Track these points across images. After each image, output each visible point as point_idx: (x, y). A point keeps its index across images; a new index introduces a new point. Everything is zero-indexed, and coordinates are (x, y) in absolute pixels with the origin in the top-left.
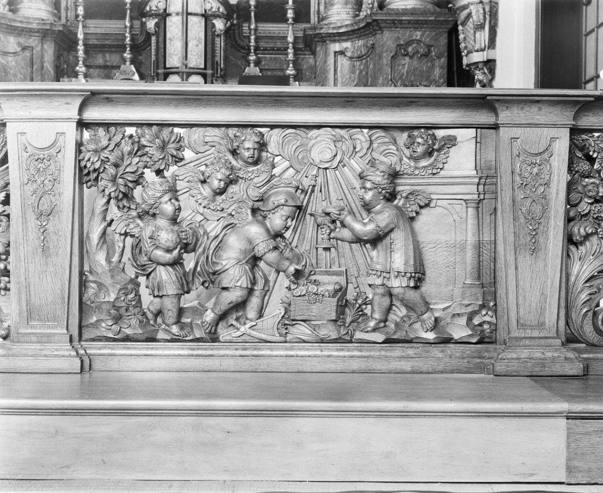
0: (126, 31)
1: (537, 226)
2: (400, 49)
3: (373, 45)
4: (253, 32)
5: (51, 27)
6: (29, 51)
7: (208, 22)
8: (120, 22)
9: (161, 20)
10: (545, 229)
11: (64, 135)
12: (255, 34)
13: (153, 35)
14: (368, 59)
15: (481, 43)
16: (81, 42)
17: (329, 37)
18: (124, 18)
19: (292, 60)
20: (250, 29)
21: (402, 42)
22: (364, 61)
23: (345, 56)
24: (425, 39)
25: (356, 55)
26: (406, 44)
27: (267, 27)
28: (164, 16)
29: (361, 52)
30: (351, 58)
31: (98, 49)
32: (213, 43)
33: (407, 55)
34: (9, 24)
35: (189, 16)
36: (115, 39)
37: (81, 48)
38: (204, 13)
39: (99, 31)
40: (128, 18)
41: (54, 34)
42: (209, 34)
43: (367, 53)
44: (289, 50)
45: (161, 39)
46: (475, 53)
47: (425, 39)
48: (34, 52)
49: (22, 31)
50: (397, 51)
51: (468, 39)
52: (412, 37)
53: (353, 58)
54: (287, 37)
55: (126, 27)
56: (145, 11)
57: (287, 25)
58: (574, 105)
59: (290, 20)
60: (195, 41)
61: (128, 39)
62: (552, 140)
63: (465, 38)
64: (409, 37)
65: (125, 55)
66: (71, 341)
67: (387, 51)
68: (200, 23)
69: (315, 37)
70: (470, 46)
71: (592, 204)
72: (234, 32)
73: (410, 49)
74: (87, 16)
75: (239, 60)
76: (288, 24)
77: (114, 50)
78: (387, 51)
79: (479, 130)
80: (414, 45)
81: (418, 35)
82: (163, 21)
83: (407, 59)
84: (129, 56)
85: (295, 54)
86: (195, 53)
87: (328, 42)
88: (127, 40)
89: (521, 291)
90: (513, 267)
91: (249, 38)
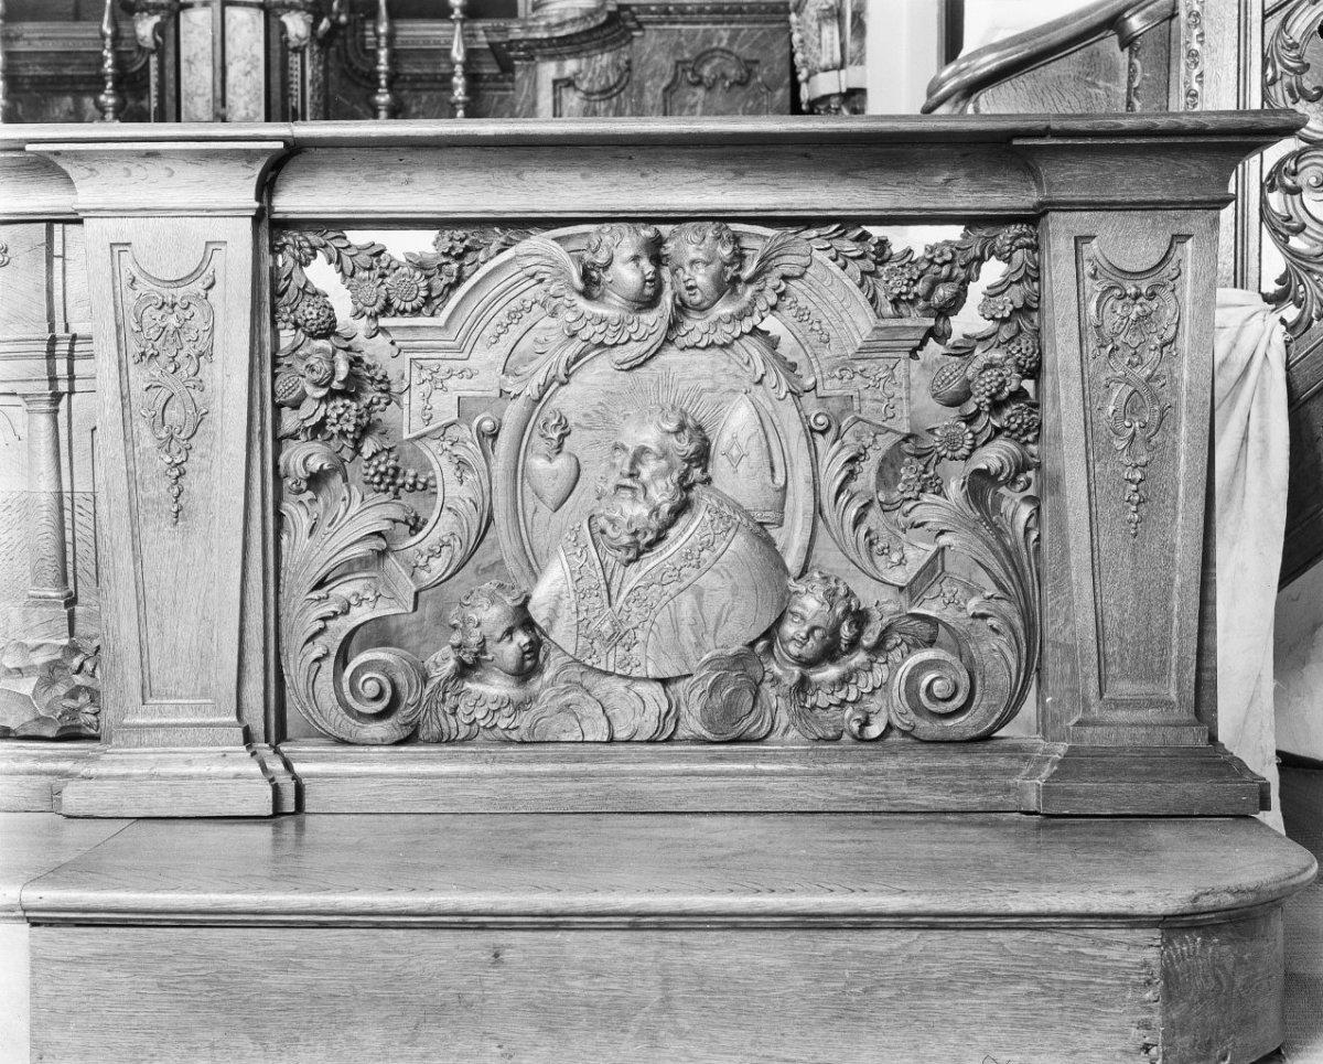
0: (104, 46)
1: (184, 453)
2: (684, 70)
3: (629, 62)
4: (383, 41)
7: (272, 20)
9: (169, 17)
10: (206, 463)
11: (223, 248)
12: (390, 44)
13: (153, 52)
14: (622, 94)
15: (832, 53)
17: (539, 47)
18: (101, 19)
19: (464, 102)
20: (377, 35)
21: (687, 56)
22: (614, 100)
23: (576, 89)
24: (740, 46)
25: (597, 87)
26: (698, 58)
27: (419, 29)
29: (608, 79)
30: (588, 93)
31: (50, 87)
32: (285, 67)
33: (699, 83)
36: (84, 64)
39: (50, 47)
40: (106, 17)
42: (276, 46)
43: (619, 81)
44: (455, 80)
45: (170, 60)
46: (821, 76)
47: (740, 46)
50: (676, 75)
51: (808, 42)
52: (711, 43)
53: (592, 94)
54: (449, 50)
55: (103, 36)
57: (451, 25)
58: (249, 162)
59: (457, 11)
60: (243, 63)
61: (110, 62)
62: (212, 247)
63: (802, 41)
64: (703, 45)
65: (102, 98)
66: (248, 738)
67: (653, 75)
68: (254, 23)
69: (510, 49)
70: (811, 60)
71: (322, 400)
72: (345, 44)
73: (706, 71)
74: (472, 12)
75: (358, 103)
76: (452, 21)
78: (653, 75)
79: (57, 228)
80: (716, 61)
81: (723, 33)
82: (173, 20)
83: (700, 92)
84: (111, 101)
85: (469, 90)
86: (242, 91)
87: (537, 59)
88: (106, 66)
89: (151, 612)
90: (128, 554)
91: (374, 55)
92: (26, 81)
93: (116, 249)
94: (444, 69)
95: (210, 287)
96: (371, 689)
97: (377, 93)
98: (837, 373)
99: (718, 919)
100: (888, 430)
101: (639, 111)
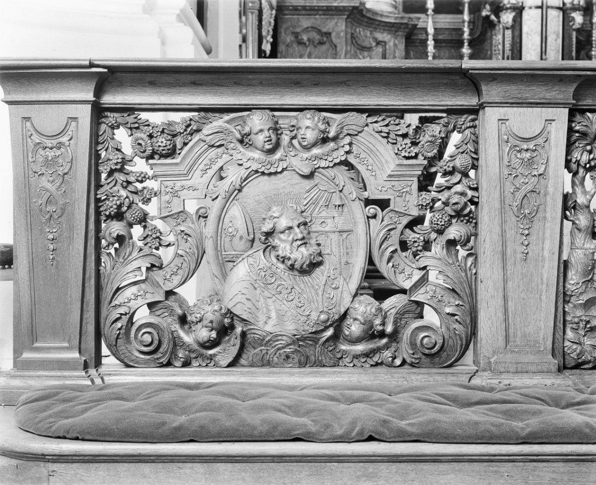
5: (408, 21)
6: (381, 46)
8: (460, 16)
16: (430, 37)
18: (461, 12)
28: (519, 10)
34: (372, 17)
35: (548, 10)
37: (431, 43)
38: (561, 6)
41: (407, 28)
45: (517, 33)
48: (387, 47)
49: (379, 25)
55: (464, 22)
56: (501, 5)
74: (437, 10)
77: (444, 45)
92: (418, 41)
93: (500, 122)
94: (423, 37)
95: (71, 139)
96: (147, 338)
97: (592, 51)
98: (380, 188)
99: (169, 458)
100: (406, 214)
101: (335, 56)
